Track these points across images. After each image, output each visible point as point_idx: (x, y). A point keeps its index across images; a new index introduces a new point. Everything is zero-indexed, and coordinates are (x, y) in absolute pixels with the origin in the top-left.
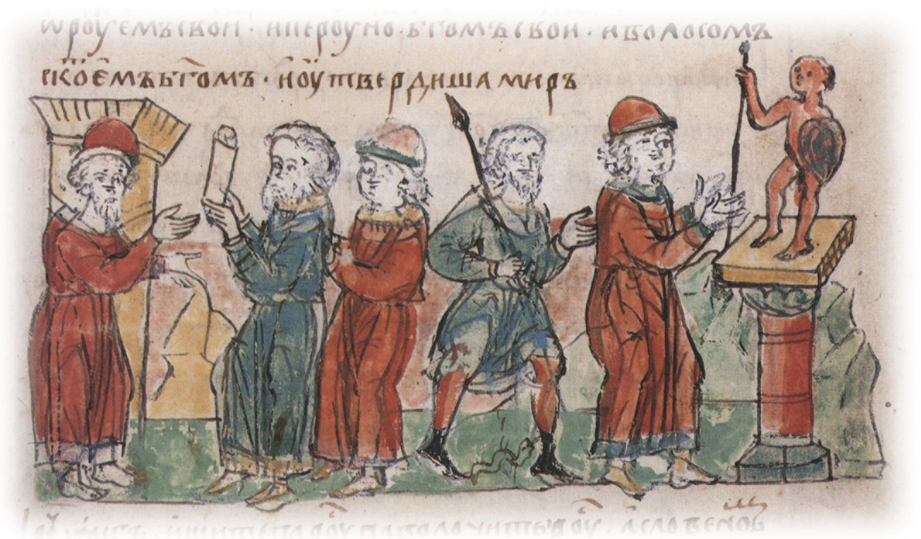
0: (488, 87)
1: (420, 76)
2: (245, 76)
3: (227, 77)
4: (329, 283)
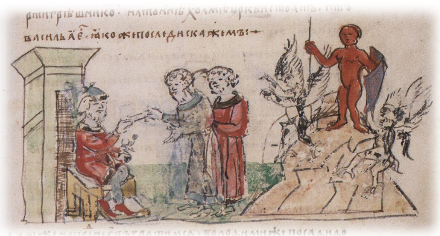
0: (182, 36)
1: (171, 32)
2: (239, 32)
3: (231, 32)
4: (361, 120)
